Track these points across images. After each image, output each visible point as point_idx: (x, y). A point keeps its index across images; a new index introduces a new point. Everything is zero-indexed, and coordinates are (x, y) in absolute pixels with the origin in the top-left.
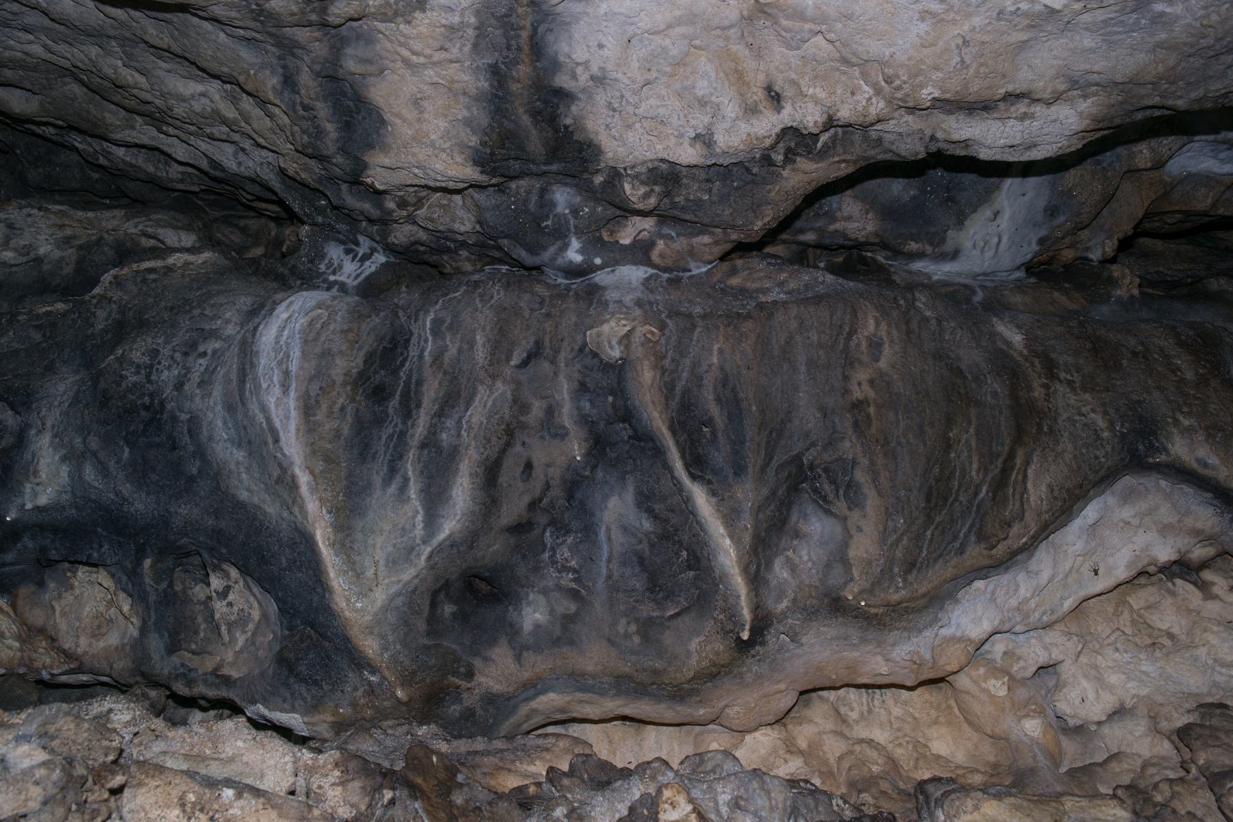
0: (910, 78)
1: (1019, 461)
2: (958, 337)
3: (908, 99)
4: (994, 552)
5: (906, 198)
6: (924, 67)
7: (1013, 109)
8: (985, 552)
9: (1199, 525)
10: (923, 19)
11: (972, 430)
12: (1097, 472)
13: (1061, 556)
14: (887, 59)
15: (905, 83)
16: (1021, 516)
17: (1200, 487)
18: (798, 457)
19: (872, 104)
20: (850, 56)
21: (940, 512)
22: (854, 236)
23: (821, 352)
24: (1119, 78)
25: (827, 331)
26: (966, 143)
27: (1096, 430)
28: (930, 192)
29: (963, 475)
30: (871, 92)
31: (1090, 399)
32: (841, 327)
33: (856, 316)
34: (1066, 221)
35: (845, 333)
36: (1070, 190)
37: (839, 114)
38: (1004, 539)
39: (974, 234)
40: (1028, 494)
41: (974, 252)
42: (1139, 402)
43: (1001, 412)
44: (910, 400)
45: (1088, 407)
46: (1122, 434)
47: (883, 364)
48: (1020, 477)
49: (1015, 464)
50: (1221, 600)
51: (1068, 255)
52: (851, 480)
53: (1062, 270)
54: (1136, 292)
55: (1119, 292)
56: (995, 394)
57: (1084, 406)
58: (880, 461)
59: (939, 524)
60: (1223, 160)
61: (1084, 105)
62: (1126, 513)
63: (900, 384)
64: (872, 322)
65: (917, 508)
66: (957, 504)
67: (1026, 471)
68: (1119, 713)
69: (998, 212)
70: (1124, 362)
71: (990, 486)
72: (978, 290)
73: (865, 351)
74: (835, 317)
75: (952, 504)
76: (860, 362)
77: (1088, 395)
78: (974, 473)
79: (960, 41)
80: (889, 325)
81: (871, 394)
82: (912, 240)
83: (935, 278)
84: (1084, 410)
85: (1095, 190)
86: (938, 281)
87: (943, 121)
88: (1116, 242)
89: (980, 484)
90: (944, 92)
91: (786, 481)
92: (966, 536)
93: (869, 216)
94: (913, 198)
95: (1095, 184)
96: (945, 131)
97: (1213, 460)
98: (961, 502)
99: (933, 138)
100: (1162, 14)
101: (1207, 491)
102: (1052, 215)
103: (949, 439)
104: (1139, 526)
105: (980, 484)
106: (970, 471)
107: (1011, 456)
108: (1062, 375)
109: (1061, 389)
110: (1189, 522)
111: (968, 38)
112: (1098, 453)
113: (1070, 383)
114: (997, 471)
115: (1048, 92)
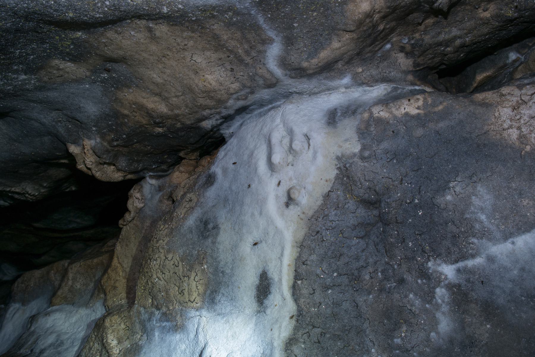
34: (185, 218)
36: (191, 268)
39: (315, 157)
41: (305, 130)
53: (182, 154)
54: (73, 149)
55: (93, 142)
68: (143, 199)
69: (287, 205)
72: (278, 72)
82: (417, 117)
83: (346, 80)
86: (341, 74)
88: (130, 206)
93: (514, 134)
94: (444, 188)
102: (206, 223)
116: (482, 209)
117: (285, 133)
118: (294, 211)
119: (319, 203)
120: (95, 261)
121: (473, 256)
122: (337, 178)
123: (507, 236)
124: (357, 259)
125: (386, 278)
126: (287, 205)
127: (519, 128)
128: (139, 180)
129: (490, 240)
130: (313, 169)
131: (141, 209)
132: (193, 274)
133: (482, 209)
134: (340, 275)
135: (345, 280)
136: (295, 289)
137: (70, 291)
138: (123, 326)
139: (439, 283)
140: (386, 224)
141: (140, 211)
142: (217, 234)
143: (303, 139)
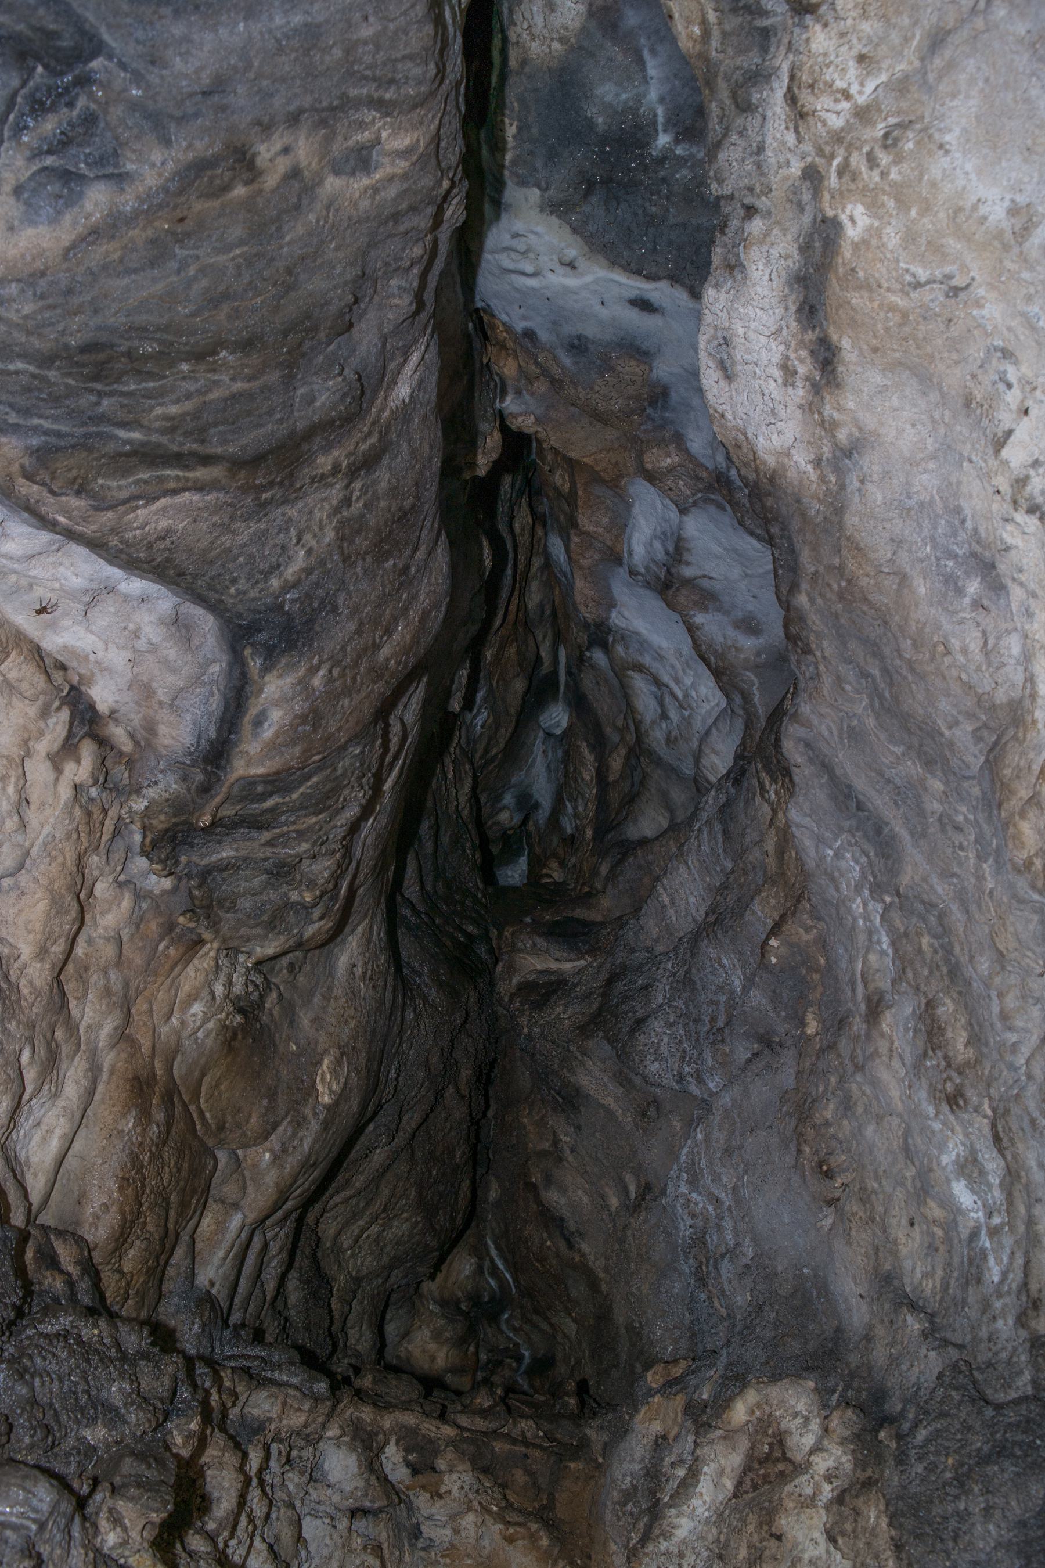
0: (894, 184)
1: (200, 473)
2: (396, 301)
3: (846, 178)
4: (22, 481)
5: (591, 111)
6: (913, 213)
7: (804, 353)
8: (15, 468)
9: (162, 729)
10: (1013, 211)
11: (239, 386)
12: (211, 588)
13: (51, 559)
14: (937, 136)
15: (884, 175)
16: (102, 504)
17: (222, 720)
18: (98, 48)
19: (837, 101)
20: (948, 53)
21: (69, 374)
22: (518, 17)
23: (337, 53)
24: (851, 520)
25: (381, 56)
26: (734, 267)
27: (278, 566)
28: (602, 152)
29: (149, 395)
30: (861, 100)
31: (327, 540)
32: (392, 81)
33: (415, 107)
34: (563, 368)
35: (380, 92)
37: (818, 27)
38: (52, 492)
40: (145, 506)
41: (508, 236)
42: (335, 609)
43: (281, 421)
44: (272, 259)
45: (313, 543)
46: (281, 606)
47: (332, 184)
48: (172, 485)
49: (194, 469)
50: (57, 779)
51: (508, 368)
52: (81, 178)
56: (310, 399)
57: (315, 536)
58: (137, 234)
59: (44, 379)
60: (651, 545)
61: (801, 460)
62: (152, 632)
63: (300, 230)
64: (407, 141)
65: (63, 333)
66: (93, 398)
67: (185, 489)
68: (525, 414)
69: (574, 268)
70: (391, 562)
71: (144, 444)
73: (351, 143)
74: (409, 64)
75: (92, 391)
76: (329, 140)
77: (333, 534)
78: (159, 411)
79: (958, 281)
80: (405, 176)
81: (270, 181)
84: (307, 537)
85: (613, 402)
87: (784, 231)
88: (532, 431)
89: (142, 426)
90: (856, 246)
91: (35, 29)
92: (36, 430)
93: (556, 45)
94: (591, 124)
95: (621, 401)
96: (767, 235)
97: (268, 732)
98: (98, 404)
99: (750, 211)
100: (960, 592)
101: (219, 729)
102: (572, 346)
103: (214, 353)
104: (135, 650)
105: (142, 426)
106: (161, 405)
107: (207, 460)
108: (357, 485)
109: (335, 493)
110: (164, 715)
111: (962, 295)
112: (242, 581)
113: (347, 502)
114: (175, 448)
115: (835, 415)
116: (617, 95)
117: (505, 254)
118: (582, 264)
119: (579, 239)
120: (580, 493)
121: (655, 115)
122: (559, 217)
123: (645, 80)
124: (636, 214)
125: (659, 192)
126: (574, 268)
127: (552, 40)
128: (501, 415)
129: (645, 96)
130: (546, 237)
131: (536, 419)
132: (619, 368)
133: (617, 95)
134: (646, 234)
135: (651, 230)
136: (651, 278)
137: (610, 531)
138: (655, 450)
139: (672, 151)
140: (611, 180)
141: (538, 421)
142: (586, 337)
143: (516, 240)
